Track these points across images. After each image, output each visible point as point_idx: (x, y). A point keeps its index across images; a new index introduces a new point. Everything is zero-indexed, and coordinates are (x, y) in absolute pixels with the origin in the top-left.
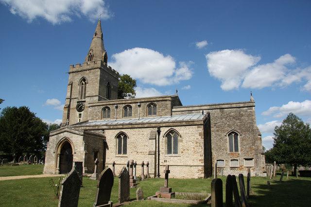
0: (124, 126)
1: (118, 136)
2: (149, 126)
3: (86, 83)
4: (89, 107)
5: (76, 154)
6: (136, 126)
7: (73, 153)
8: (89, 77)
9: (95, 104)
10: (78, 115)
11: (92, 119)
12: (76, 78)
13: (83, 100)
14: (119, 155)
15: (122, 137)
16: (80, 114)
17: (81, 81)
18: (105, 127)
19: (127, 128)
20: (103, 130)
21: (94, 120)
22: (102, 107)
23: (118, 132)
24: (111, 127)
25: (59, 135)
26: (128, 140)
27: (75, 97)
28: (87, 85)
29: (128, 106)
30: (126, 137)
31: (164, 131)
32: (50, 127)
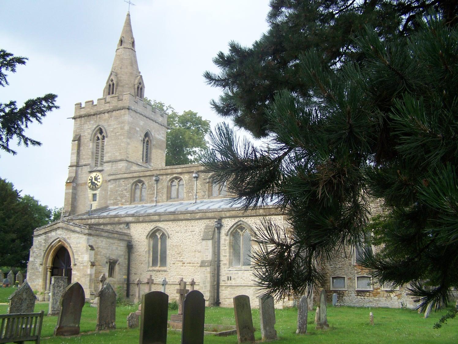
0: (161, 217)
1: (152, 235)
2: (203, 215)
3: (104, 137)
4: (109, 181)
5: (76, 267)
6: (182, 217)
7: (72, 265)
8: (109, 125)
9: (119, 176)
10: (91, 196)
11: (115, 204)
12: (86, 127)
13: (99, 168)
14: (155, 268)
15: (159, 237)
16: (94, 195)
17: (95, 134)
18: (130, 219)
19: (167, 221)
20: (128, 224)
21: (117, 205)
22: (132, 181)
23: (152, 228)
24: (140, 219)
25: (49, 234)
26: (169, 242)
27: (84, 163)
28: (106, 139)
29: (176, 178)
30: (164, 237)
31: (228, 224)
32: (55, 215)
